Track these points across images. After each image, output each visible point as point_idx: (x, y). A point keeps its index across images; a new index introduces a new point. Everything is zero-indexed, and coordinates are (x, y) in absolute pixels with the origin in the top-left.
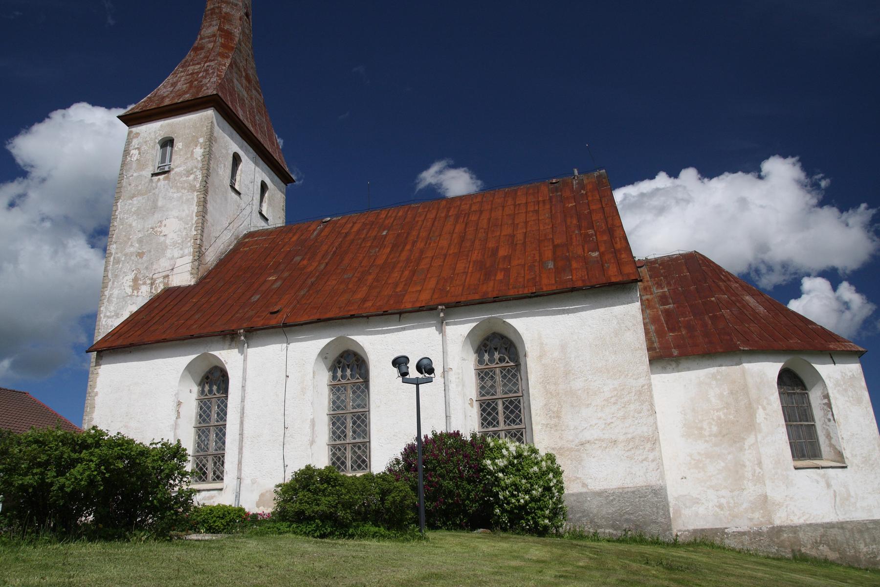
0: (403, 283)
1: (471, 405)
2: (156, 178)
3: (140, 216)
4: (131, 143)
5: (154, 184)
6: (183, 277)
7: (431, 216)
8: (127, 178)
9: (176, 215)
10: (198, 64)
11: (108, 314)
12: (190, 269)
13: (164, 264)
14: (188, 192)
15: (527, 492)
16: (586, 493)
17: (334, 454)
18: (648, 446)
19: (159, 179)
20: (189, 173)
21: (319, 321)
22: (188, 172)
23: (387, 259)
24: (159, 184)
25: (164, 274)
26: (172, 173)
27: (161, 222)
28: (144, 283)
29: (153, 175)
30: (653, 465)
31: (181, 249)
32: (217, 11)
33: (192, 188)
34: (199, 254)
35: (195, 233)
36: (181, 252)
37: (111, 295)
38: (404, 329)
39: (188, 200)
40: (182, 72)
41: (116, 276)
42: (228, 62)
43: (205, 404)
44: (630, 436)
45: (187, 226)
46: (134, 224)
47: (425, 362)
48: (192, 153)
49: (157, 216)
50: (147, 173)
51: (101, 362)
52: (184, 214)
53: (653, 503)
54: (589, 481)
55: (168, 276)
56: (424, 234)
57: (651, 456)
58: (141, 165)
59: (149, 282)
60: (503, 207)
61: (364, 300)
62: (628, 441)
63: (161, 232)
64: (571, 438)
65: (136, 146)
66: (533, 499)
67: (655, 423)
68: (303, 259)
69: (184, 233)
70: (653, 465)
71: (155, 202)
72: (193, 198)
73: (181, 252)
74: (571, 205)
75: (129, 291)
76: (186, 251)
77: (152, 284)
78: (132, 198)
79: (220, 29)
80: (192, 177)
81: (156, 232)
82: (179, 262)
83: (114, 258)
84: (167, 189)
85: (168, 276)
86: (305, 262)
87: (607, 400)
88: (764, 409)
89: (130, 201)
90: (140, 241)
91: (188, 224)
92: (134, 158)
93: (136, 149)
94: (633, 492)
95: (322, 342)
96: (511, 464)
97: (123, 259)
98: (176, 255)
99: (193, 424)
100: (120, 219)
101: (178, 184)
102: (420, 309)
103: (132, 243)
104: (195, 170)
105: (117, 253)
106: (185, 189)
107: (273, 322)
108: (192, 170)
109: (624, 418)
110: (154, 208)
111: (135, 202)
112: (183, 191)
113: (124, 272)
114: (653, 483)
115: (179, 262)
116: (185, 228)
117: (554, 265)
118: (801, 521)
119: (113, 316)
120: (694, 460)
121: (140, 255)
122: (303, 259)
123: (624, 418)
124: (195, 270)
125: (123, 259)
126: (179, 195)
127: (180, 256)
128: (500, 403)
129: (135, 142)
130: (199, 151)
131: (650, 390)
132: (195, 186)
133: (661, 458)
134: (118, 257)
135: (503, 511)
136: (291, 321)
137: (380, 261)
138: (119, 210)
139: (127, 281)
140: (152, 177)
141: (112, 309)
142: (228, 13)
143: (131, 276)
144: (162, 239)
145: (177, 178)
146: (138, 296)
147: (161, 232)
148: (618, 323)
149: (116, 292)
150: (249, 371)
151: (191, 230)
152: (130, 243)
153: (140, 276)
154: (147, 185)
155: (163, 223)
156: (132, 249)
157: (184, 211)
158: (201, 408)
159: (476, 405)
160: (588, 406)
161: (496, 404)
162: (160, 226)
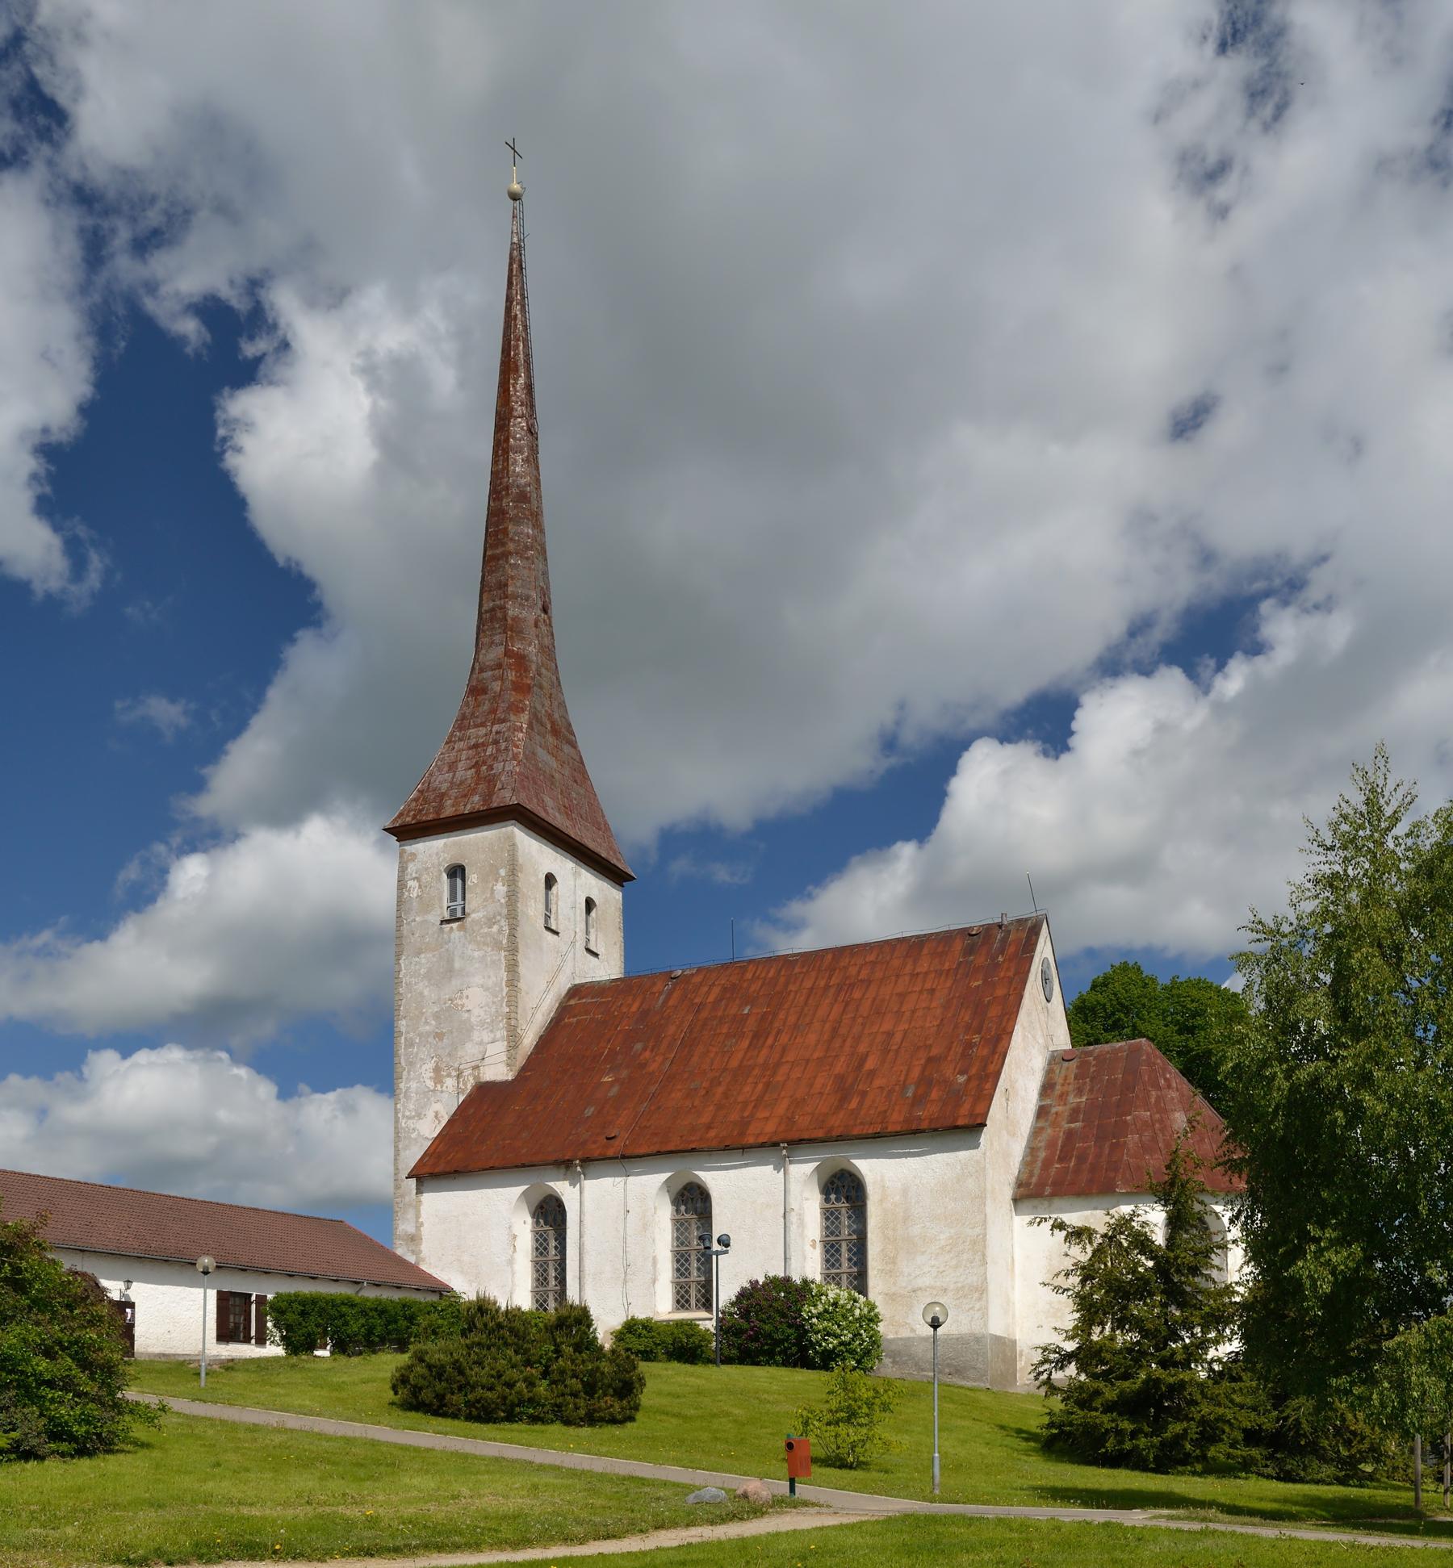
0: (753, 1104)
1: (814, 1246)
2: (447, 927)
3: (432, 982)
4: (407, 868)
5: (445, 936)
6: (498, 1071)
7: (808, 984)
8: (408, 924)
9: (481, 982)
10: (483, 725)
11: (407, 1113)
12: (505, 1059)
13: (470, 1052)
14: (493, 950)
15: (836, 1336)
16: (914, 1338)
17: (678, 1293)
18: (976, 1295)
19: (452, 928)
20: (491, 922)
21: (659, 1153)
22: (489, 920)
23: (742, 1062)
24: (453, 935)
25: (473, 1064)
26: (468, 920)
27: (461, 991)
28: (449, 1075)
29: (442, 922)
30: (978, 1315)
31: (492, 1031)
32: (499, 615)
33: (497, 945)
35: (508, 1010)
36: (492, 1035)
37: (409, 1088)
38: (746, 1165)
39: (493, 962)
40: (460, 740)
41: (411, 1064)
42: (525, 717)
43: (541, 1236)
44: (960, 1285)
45: (495, 1000)
46: (426, 992)
47: (724, 1238)
48: (492, 891)
49: (456, 983)
50: (434, 917)
51: (422, 1189)
52: (490, 983)
53: (974, 1350)
54: (918, 1326)
55: (477, 1067)
56: (792, 1019)
57: (977, 1306)
58: (426, 907)
59: (454, 1073)
60: (898, 976)
61: (709, 1127)
62: (958, 1290)
63: (463, 1006)
64: (904, 1284)
65: (414, 875)
66: (842, 1344)
67: (985, 1273)
68: (644, 1049)
69: (493, 1010)
70: (978, 1315)
71: (450, 961)
72: (500, 960)
73: (492, 1035)
74: (976, 984)
75: (430, 1084)
76: (498, 1034)
77: (458, 1077)
78: (418, 954)
79: (508, 653)
80: (495, 928)
81: (457, 1005)
82: (491, 1050)
83: (406, 1038)
84: (464, 944)
85: (477, 1067)
86: (647, 1054)
87: (942, 1248)
89: (417, 959)
91: (497, 997)
92: (414, 894)
93: (414, 879)
94: (957, 1339)
95: (665, 1176)
96: (826, 1311)
97: (417, 1041)
98: (486, 1039)
99: (530, 1258)
100: (406, 983)
101: (479, 938)
102: (762, 1145)
103: (426, 1019)
104: (498, 918)
105: (407, 1032)
106: (488, 945)
107: (610, 1153)
108: (494, 917)
109: (957, 1267)
110: (450, 972)
111: (423, 961)
112: (485, 948)
113: (422, 1059)
114: (977, 1332)
115: (491, 1050)
116: (494, 1003)
119: (414, 1117)
120: (1053, 1308)
122: (644, 1049)
123: (957, 1267)
125: (417, 1041)
126: (481, 953)
127: (490, 1040)
128: (844, 1244)
129: (412, 868)
130: (501, 889)
131: (984, 1240)
132: (501, 943)
133: (987, 1308)
134: (411, 1038)
135: (816, 1352)
136: (628, 1153)
137: (734, 1063)
138: (404, 971)
139: (427, 1070)
140: (441, 924)
141: (412, 1107)
142: (516, 617)
143: (431, 1065)
145: (475, 928)
146: (442, 1092)
147: (463, 1006)
148: (962, 1168)
149: (414, 1085)
150: (587, 1204)
151: (502, 1006)
152: (423, 1020)
153: (443, 1066)
154: (436, 936)
155: (465, 993)
156: (427, 1028)
157: (489, 977)
158: (537, 1241)
159: (819, 1246)
160: (923, 1253)
161: (840, 1246)
162: (461, 998)
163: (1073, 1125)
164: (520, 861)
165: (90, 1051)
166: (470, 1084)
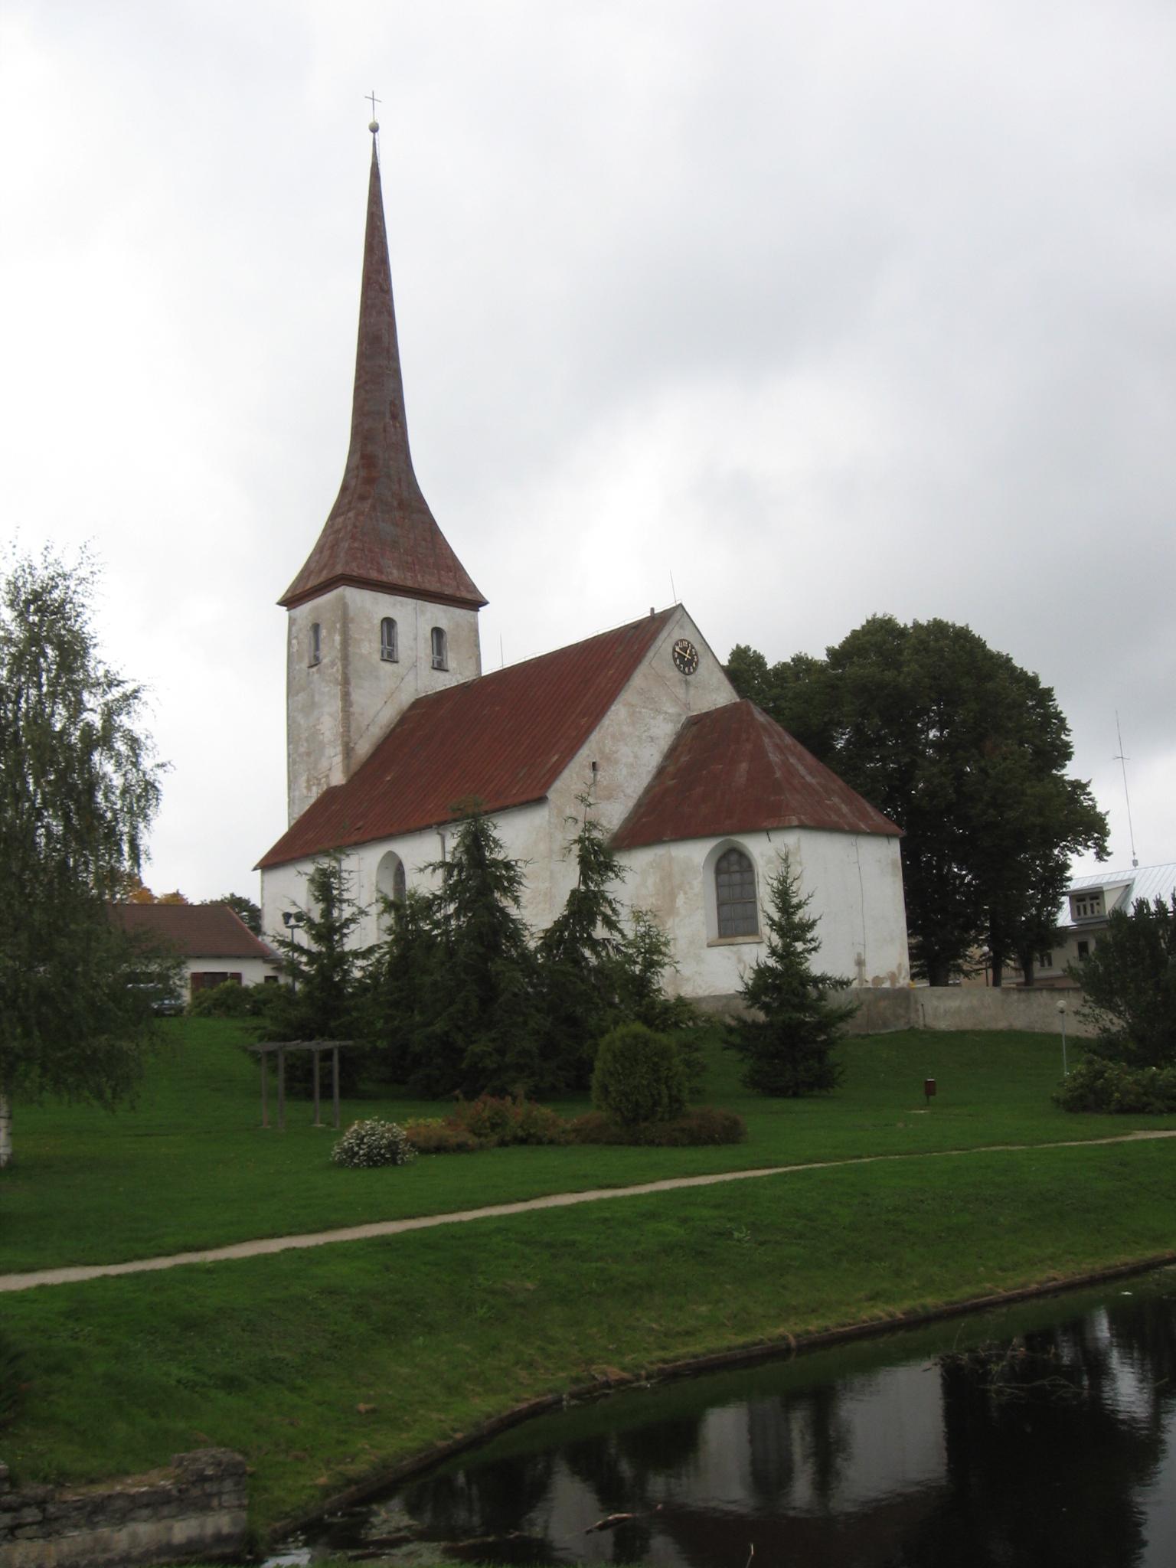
6: (338, 778)
25: (324, 774)
34: (348, 751)
75: (305, 791)
88: (686, 893)
90: (307, 740)
117: (285, 966)
118: (706, 993)
121: (308, 754)
124: (346, 768)
130: (337, 638)
143: (304, 778)
144: (321, 737)
155: (321, 720)
163: (1161, 1382)
164: (351, 614)
165: (770, 666)
166: (325, 787)
